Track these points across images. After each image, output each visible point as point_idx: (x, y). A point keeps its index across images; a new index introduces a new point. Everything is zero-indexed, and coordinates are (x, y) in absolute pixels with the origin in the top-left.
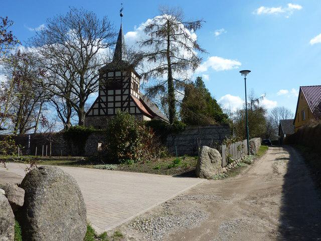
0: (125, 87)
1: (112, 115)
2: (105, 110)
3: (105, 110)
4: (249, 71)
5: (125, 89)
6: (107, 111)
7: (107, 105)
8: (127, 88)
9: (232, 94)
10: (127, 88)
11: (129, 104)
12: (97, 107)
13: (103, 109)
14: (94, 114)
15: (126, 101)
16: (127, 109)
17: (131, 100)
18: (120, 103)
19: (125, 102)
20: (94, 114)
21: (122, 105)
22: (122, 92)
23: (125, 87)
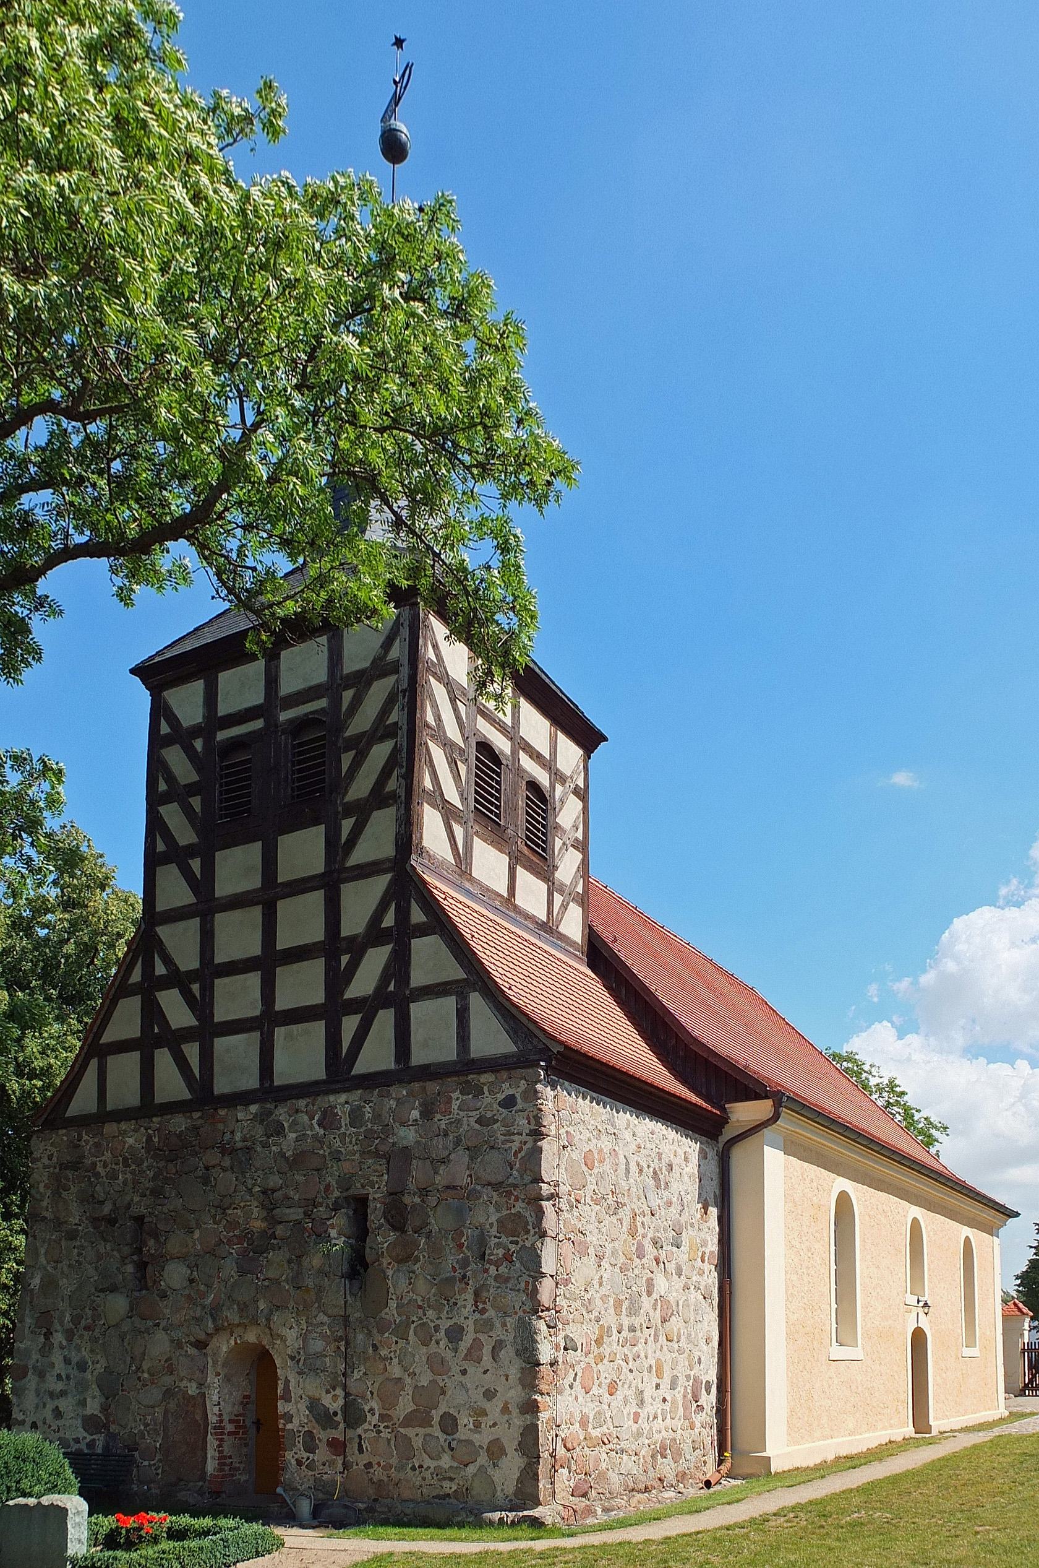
0: (361, 788)
1: (241, 1098)
2: (191, 1052)
3: (191, 1052)
4: (1017, 1214)
5: (362, 811)
6: (207, 1056)
7: (202, 1006)
8: (379, 798)
9: (279, 1524)
10: (379, 798)
11: (399, 965)
12: (317, 996)
13: (174, 1040)
14: (419, 1057)
15: (375, 935)
16: (385, 1019)
17: (417, 916)
18: (314, 971)
19: (358, 948)
20: (419, 1057)
21: (336, 980)
22: (336, 849)
23: (361, 788)
